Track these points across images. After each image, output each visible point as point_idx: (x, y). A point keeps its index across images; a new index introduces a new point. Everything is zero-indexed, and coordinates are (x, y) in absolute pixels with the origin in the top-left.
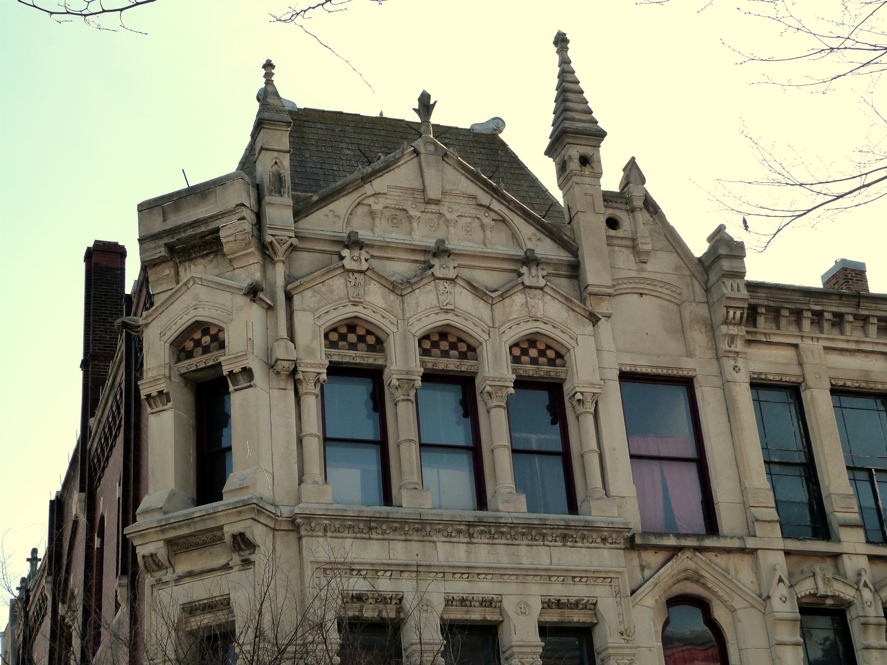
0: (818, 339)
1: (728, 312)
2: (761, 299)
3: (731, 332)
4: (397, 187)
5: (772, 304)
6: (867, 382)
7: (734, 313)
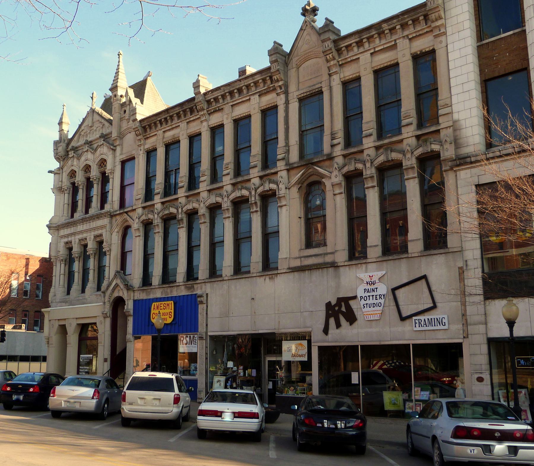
0: (161, 129)
1: (327, 58)
2: (145, 124)
3: (139, 138)
4: (86, 126)
5: (149, 123)
6: (174, 139)
7: (329, 56)
